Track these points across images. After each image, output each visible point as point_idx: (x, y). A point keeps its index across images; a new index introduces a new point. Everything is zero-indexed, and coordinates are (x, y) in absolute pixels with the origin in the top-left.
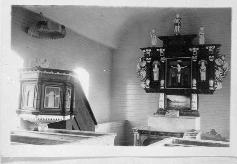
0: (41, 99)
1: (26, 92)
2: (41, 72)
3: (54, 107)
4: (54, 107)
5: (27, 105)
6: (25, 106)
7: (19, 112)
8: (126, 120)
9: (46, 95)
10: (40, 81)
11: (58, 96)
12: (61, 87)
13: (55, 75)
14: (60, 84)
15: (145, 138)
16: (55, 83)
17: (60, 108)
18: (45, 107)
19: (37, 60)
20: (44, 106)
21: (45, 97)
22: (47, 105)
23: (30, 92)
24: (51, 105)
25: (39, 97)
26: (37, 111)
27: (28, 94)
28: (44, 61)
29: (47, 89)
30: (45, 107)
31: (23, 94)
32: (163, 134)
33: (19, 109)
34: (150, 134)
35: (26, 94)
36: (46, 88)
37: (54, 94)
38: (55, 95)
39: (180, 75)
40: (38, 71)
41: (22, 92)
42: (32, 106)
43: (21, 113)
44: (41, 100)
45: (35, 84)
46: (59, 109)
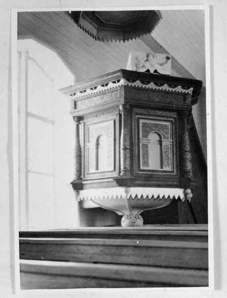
0: (133, 151)
1: (91, 139)
2: (130, 84)
3: (162, 168)
4: (162, 168)
5: (97, 169)
6: (92, 170)
7: (78, 186)
8: (172, 70)
9: (143, 141)
11: (167, 142)
12: (172, 121)
13: (159, 91)
14: (169, 114)
18: (142, 168)
19: (148, 56)
20: (139, 167)
21: (141, 146)
22: (146, 163)
23: (100, 140)
24: (153, 163)
25: (128, 143)
26: (129, 176)
27: (98, 144)
28: (165, 59)
29: (142, 127)
30: (142, 168)
31: (84, 147)
33: (78, 179)
35: (92, 145)
36: (141, 125)
37: (158, 138)
38: (160, 142)
40: (123, 82)
41: (81, 137)
42: (113, 169)
43: (82, 188)
44: (131, 150)
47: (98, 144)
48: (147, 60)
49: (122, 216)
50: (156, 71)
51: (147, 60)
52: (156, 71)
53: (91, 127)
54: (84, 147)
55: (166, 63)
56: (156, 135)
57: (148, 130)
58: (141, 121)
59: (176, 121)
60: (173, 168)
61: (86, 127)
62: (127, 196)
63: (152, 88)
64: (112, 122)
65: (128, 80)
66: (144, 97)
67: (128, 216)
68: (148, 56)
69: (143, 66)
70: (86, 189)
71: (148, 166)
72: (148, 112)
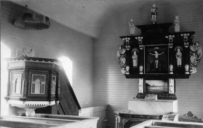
0: (28, 87)
2: (28, 61)
4: (40, 93)
5: (15, 92)
9: (33, 83)
10: (27, 69)
11: (44, 83)
13: (41, 63)
15: (126, 121)
16: (42, 71)
17: (46, 95)
19: (23, 50)
22: (34, 92)
24: (37, 91)
26: (25, 98)
27: (16, 82)
31: (11, 82)
32: (143, 117)
34: (131, 117)
35: (14, 82)
37: (40, 81)
39: (157, 61)
42: (20, 93)
44: (28, 87)
45: (22, 72)
46: (45, 95)
47: (16, 82)
48: (23, 52)
49: (26, 111)
50: (26, 56)
51: (23, 52)
52: (26, 56)
53: (14, 75)
54: (11, 82)
55: (31, 52)
56: (40, 80)
57: (35, 79)
58: (33, 75)
59: (48, 74)
60: (45, 94)
61: (12, 74)
62: (24, 105)
63: (43, 63)
64: (21, 74)
65: (27, 60)
66: (39, 66)
67: (28, 111)
68: (32, 50)
69: (21, 54)
70: (11, 100)
71: (34, 92)
72: (36, 71)
